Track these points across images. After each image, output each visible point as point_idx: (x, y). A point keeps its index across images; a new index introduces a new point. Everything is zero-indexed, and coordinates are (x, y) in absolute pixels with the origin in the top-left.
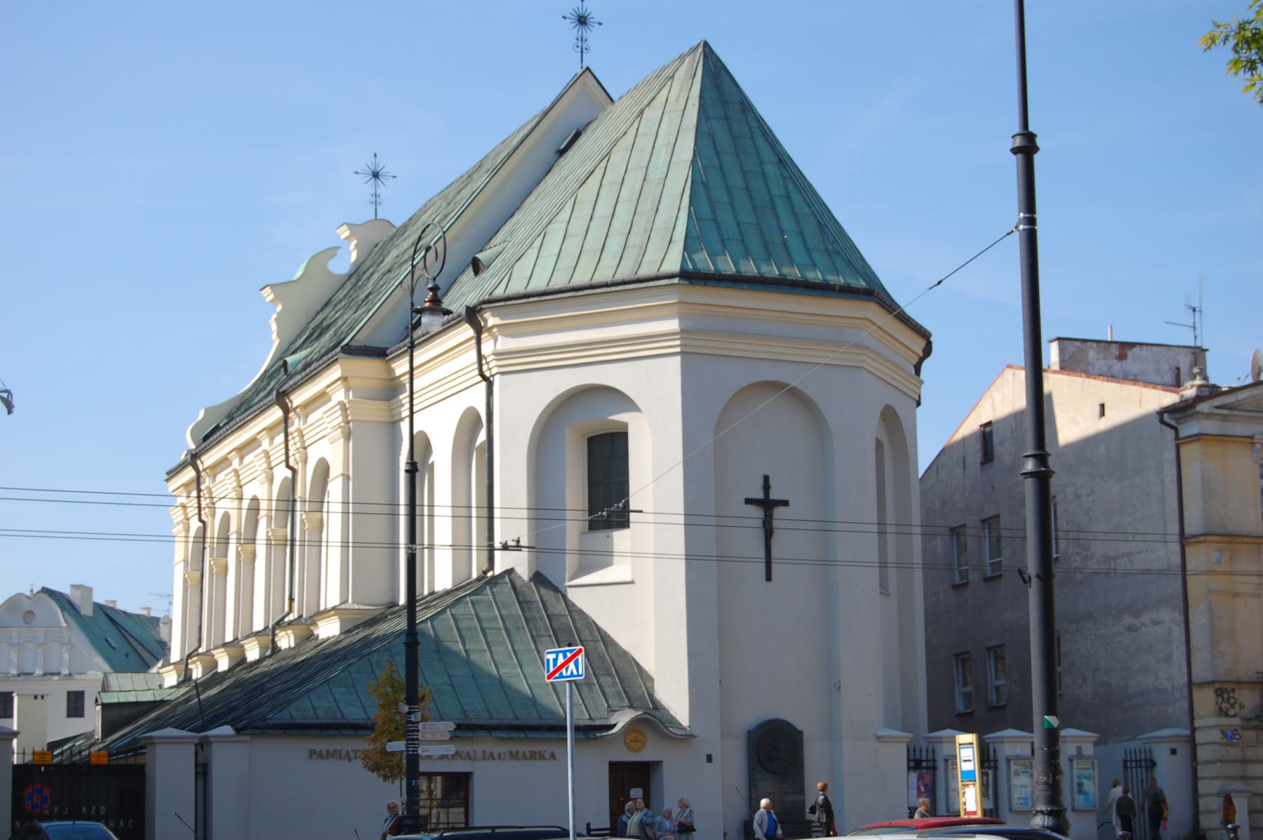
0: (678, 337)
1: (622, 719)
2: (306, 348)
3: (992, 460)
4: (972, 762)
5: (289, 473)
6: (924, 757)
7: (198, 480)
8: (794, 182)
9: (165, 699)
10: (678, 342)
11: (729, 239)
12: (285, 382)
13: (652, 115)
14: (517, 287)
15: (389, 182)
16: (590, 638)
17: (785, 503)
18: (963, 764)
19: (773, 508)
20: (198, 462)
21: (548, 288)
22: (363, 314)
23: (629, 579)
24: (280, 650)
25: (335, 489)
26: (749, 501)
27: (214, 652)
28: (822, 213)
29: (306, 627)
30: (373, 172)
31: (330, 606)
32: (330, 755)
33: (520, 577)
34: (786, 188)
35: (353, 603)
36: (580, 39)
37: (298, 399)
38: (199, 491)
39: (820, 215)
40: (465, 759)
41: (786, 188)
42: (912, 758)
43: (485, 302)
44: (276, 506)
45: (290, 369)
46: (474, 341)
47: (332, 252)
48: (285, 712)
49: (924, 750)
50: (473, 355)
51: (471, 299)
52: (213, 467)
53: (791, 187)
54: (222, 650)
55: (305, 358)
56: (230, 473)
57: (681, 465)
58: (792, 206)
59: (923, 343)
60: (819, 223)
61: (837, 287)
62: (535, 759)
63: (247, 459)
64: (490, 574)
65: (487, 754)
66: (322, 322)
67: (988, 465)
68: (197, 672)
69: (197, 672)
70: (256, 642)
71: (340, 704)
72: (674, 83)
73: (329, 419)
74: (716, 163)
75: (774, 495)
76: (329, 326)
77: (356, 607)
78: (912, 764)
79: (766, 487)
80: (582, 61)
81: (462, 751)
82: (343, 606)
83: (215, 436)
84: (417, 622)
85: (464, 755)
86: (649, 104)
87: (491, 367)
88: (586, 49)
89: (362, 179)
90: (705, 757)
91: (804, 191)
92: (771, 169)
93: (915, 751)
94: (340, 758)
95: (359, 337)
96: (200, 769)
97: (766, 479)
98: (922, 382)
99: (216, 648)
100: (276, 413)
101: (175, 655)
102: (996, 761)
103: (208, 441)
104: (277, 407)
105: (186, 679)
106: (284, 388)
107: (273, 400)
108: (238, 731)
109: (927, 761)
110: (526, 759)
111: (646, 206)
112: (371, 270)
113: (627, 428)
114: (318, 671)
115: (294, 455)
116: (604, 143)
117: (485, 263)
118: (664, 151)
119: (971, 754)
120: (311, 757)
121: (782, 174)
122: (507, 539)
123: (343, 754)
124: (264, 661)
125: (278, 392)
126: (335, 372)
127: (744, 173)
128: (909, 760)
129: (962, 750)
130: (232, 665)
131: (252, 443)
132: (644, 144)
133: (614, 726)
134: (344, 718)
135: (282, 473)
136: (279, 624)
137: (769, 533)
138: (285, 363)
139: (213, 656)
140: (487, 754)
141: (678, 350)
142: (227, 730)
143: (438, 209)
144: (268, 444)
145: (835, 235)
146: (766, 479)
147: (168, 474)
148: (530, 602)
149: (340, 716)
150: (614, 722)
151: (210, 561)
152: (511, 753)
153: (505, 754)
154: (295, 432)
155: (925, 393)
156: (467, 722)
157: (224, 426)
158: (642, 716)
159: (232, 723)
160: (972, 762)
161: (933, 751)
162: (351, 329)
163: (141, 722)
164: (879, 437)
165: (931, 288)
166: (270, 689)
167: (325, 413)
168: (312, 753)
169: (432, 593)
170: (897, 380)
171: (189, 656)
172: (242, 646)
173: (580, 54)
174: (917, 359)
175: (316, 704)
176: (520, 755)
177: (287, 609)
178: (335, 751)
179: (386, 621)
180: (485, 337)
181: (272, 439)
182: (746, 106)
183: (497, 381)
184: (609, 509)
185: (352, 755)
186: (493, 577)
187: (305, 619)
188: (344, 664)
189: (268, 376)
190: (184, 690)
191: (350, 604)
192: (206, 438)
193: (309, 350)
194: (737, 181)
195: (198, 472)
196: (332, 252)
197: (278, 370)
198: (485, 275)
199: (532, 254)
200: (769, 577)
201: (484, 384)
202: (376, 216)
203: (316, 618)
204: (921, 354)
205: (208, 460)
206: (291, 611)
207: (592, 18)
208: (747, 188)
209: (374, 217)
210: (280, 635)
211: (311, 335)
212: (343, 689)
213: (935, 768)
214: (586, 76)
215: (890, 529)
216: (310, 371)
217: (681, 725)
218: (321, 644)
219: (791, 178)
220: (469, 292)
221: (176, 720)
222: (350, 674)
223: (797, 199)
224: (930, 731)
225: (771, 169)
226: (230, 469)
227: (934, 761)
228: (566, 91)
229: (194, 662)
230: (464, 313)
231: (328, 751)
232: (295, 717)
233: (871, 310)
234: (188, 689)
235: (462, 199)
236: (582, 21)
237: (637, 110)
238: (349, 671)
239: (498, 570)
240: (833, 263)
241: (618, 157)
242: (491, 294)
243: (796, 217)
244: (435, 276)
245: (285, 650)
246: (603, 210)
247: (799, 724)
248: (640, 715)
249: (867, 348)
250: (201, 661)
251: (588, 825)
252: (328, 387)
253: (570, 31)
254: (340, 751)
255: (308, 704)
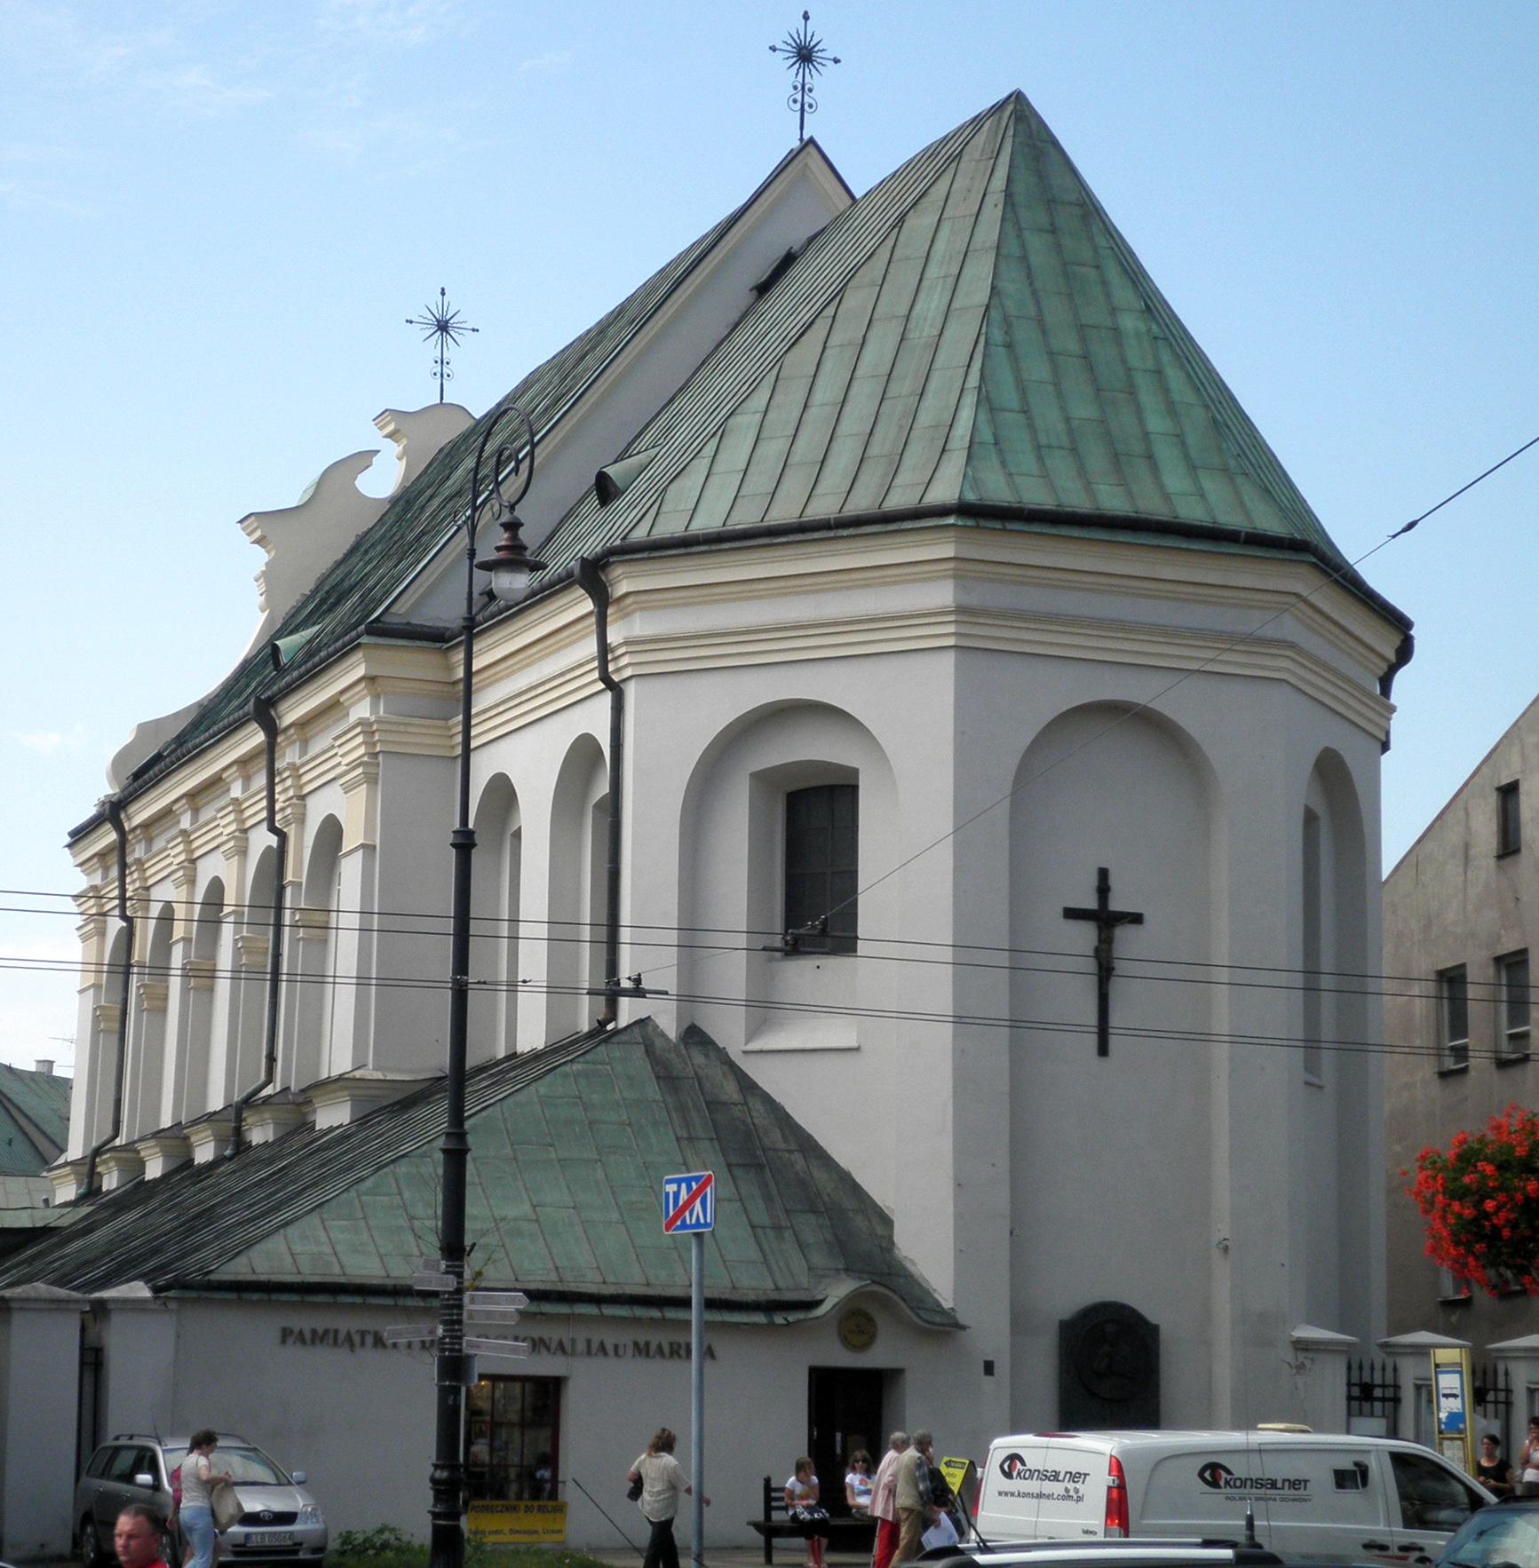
0: (952, 618)
1: (836, 1292)
2: (313, 624)
3: (1517, 851)
4: (1459, 1399)
5: (273, 841)
6: (1378, 1381)
7: (122, 847)
8: (1171, 345)
9: (51, 1225)
10: (951, 629)
11: (1050, 447)
12: (274, 681)
13: (920, 223)
14: (670, 526)
15: (465, 339)
16: (784, 1146)
17: (1137, 919)
18: (1443, 1400)
19: (1113, 926)
20: (123, 816)
21: (725, 528)
22: (410, 566)
23: (854, 1044)
24: (251, 1146)
25: (351, 870)
26: (1072, 914)
27: (139, 1146)
28: (1220, 403)
29: (299, 1103)
30: (438, 321)
31: (335, 1073)
32: (318, 1338)
33: (663, 1035)
34: (1157, 358)
35: (374, 1069)
36: (800, 88)
37: (292, 712)
38: (123, 866)
39: (1216, 406)
40: (654, 1357)
41: (1157, 358)
42: (1355, 1379)
43: (613, 552)
44: (200, 914)
45: (284, 659)
46: (593, 619)
47: (363, 459)
48: (242, 1260)
49: (1378, 1366)
50: (590, 647)
51: (591, 546)
52: (146, 825)
53: (1166, 356)
54: (152, 1143)
55: (310, 641)
56: (176, 837)
57: (860, 890)
58: (1166, 391)
59: (1396, 640)
60: (1214, 420)
61: (1243, 535)
62: (679, 1356)
63: (206, 815)
64: (610, 1027)
65: (595, 1345)
66: (343, 580)
67: (1508, 861)
68: (111, 1181)
69: (111, 1181)
70: (210, 1132)
71: (338, 1248)
72: (962, 165)
73: (342, 751)
74: (1032, 311)
75: (1117, 904)
76: (352, 589)
77: (379, 1075)
78: (1356, 1391)
79: (1103, 890)
80: (802, 128)
81: (550, 1339)
82: (358, 1074)
83: (156, 769)
84: (466, 1114)
85: (553, 1345)
86: (915, 203)
87: (622, 667)
88: (811, 106)
89: (419, 333)
90: (982, 1364)
91: (1189, 362)
92: (1130, 323)
93: (1361, 1368)
94: (335, 1343)
95: (400, 608)
96: (90, 1358)
97: (1103, 874)
98: (1392, 709)
99: (141, 1140)
100: (255, 737)
101: (75, 1150)
102: (1508, 1391)
103: (140, 781)
104: (254, 726)
105: (91, 1191)
106: (269, 693)
107: (248, 714)
108: (156, 1290)
109: (1383, 1386)
110: (304, 1342)
111: (904, 387)
112: (429, 492)
113: (857, 779)
114: (304, 1189)
115: (283, 809)
116: (835, 274)
117: (620, 484)
118: (939, 288)
119: (1458, 1385)
120: (284, 1341)
121: (1149, 330)
122: (640, 971)
123: (342, 1336)
124: (219, 1166)
125: (258, 699)
126: (355, 669)
127: (1081, 329)
128: (1349, 1384)
129: (1441, 1377)
130: (166, 1171)
131: (215, 784)
132: (905, 276)
133: (818, 1303)
134: (344, 1274)
135: (263, 840)
136: (248, 1102)
137: (1105, 971)
138: (276, 649)
139: (138, 1152)
140: (595, 1345)
141: (951, 642)
142: (139, 1290)
143: (546, 388)
144: (240, 792)
145: (1242, 443)
146: (1103, 874)
147: (73, 834)
148: (678, 1078)
149: (337, 1270)
150: (819, 1297)
151: (138, 988)
152: (636, 1344)
153: (625, 1346)
154: (285, 770)
155: (1397, 725)
156: (560, 1287)
157: (168, 756)
158: (869, 1289)
159: (146, 1277)
160: (1459, 1399)
161: (1395, 1369)
162: (388, 593)
163: (7, 1265)
164: (1311, 806)
165: (1394, 537)
166: (223, 1217)
167: (336, 739)
168: (286, 1334)
169: (510, 1057)
170: (1349, 707)
171: (97, 1152)
172: (187, 1138)
173: (799, 113)
174: (1385, 667)
175: (297, 1248)
176: (653, 1348)
177: (263, 1077)
178: (326, 1332)
179: (429, 1103)
180: (612, 614)
181: (247, 780)
182: (1090, 211)
183: (631, 691)
184: (795, 931)
185: (357, 1339)
186: (616, 1032)
187: (294, 1094)
188: (351, 1177)
189: (247, 670)
190: (85, 1210)
191: (369, 1073)
192: (137, 775)
193: (316, 628)
194: (1068, 342)
195: (122, 833)
196: (363, 459)
197: (264, 663)
198: (619, 504)
199: (701, 465)
200: (1103, 1050)
201: (608, 697)
202: (442, 398)
203: (310, 1093)
204: (1392, 657)
205: (140, 813)
206: (270, 1078)
207: (823, 50)
208: (1086, 356)
209: (439, 401)
210: (249, 1121)
211: (323, 601)
212: (345, 1223)
213: (1396, 1400)
214: (808, 154)
215: (1326, 982)
216: (315, 665)
217: (939, 1305)
218: (322, 1137)
219: (1166, 339)
220: (590, 533)
221: (63, 1264)
222: (359, 1196)
223: (1174, 376)
224: (1389, 1335)
225: (1130, 323)
226: (174, 831)
227: (1396, 1387)
228: (772, 181)
229: (105, 1162)
230: (577, 571)
231: (314, 1332)
232: (258, 1270)
233: (1300, 581)
234: (92, 1208)
235: (585, 371)
236: (805, 55)
237: (894, 214)
238: (357, 1191)
239: (624, 1019)
240: (1237, 493)
241: (857, 300)
242: (624, 538)
243: (1172, 410)
244: (513, 501)
245: (258, 1146)
246: (827, 391)
247: (1152, 1316)
248: (866, 1285)
249: (1292, 646)
250: (118, 1160)
251: (767, 1481)
252: (343, 692)
253: (784, 73)
254: (336, 1331)
255: (283, 1248)
